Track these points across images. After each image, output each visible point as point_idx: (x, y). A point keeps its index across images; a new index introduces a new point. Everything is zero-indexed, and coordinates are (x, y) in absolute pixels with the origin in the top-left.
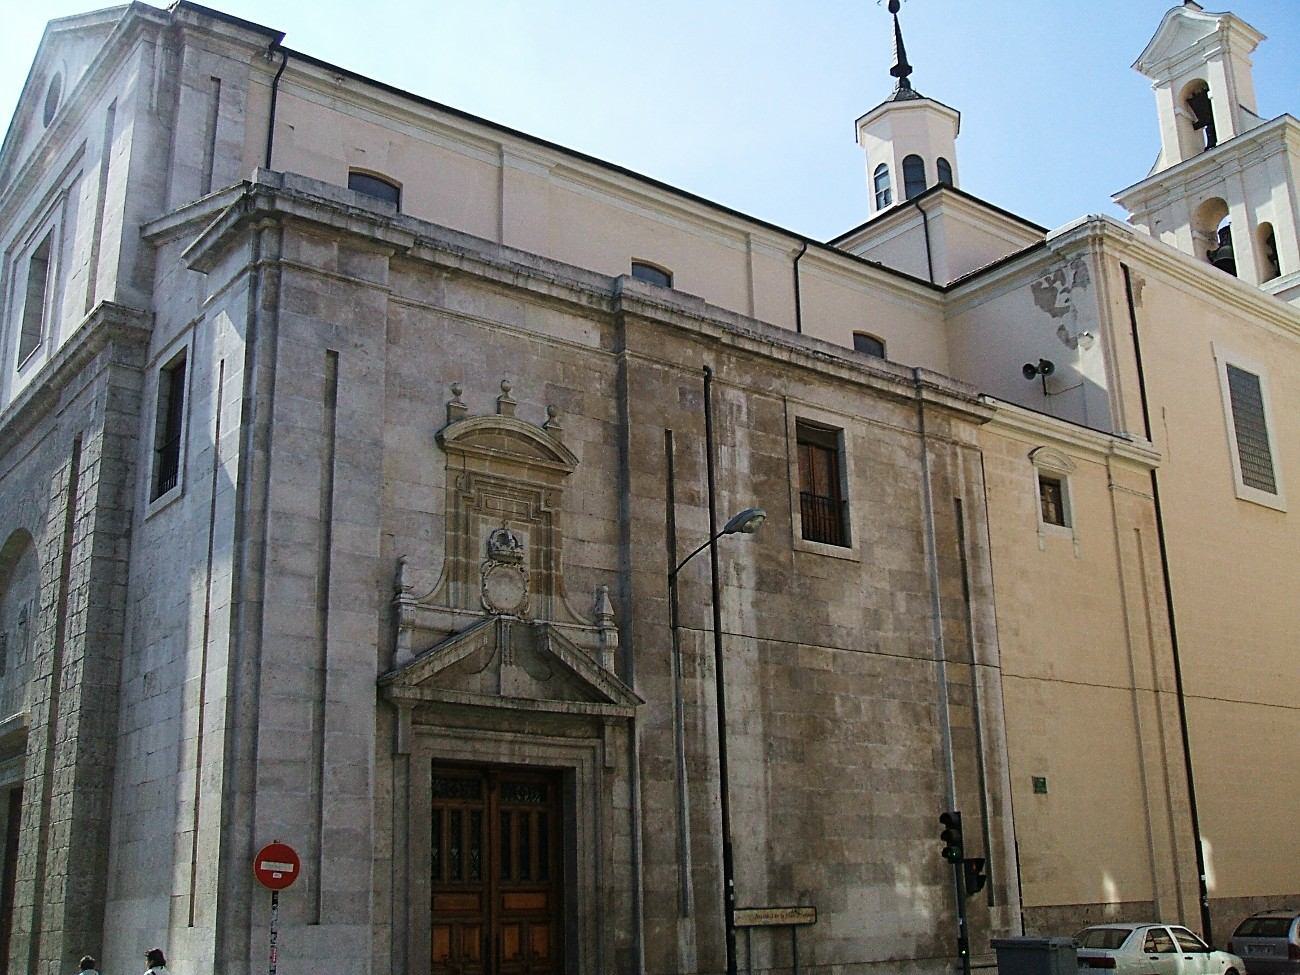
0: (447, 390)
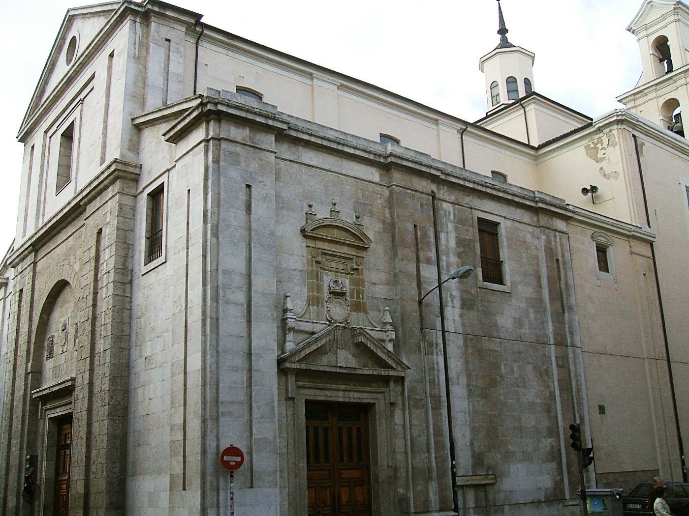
0: (305, 205)
